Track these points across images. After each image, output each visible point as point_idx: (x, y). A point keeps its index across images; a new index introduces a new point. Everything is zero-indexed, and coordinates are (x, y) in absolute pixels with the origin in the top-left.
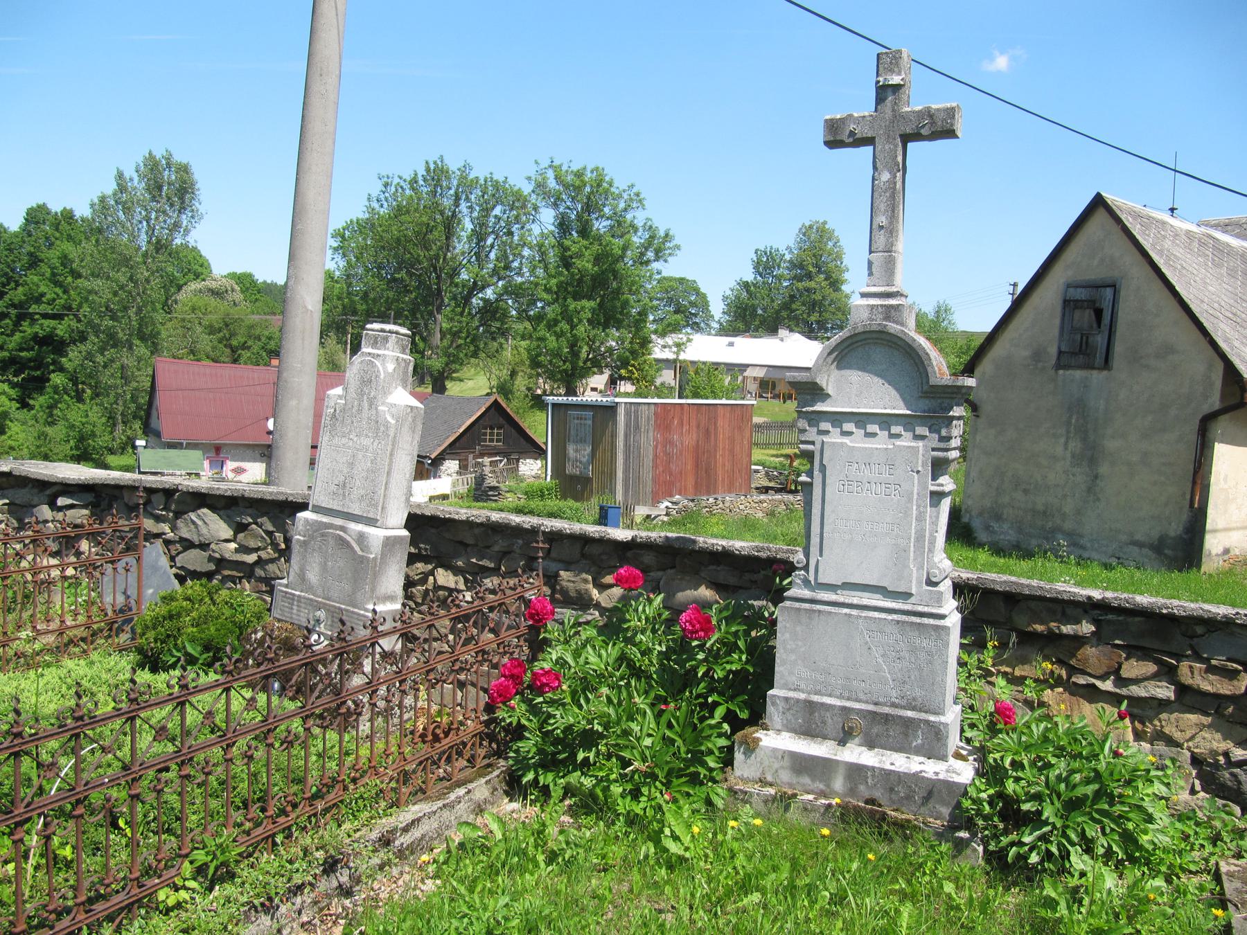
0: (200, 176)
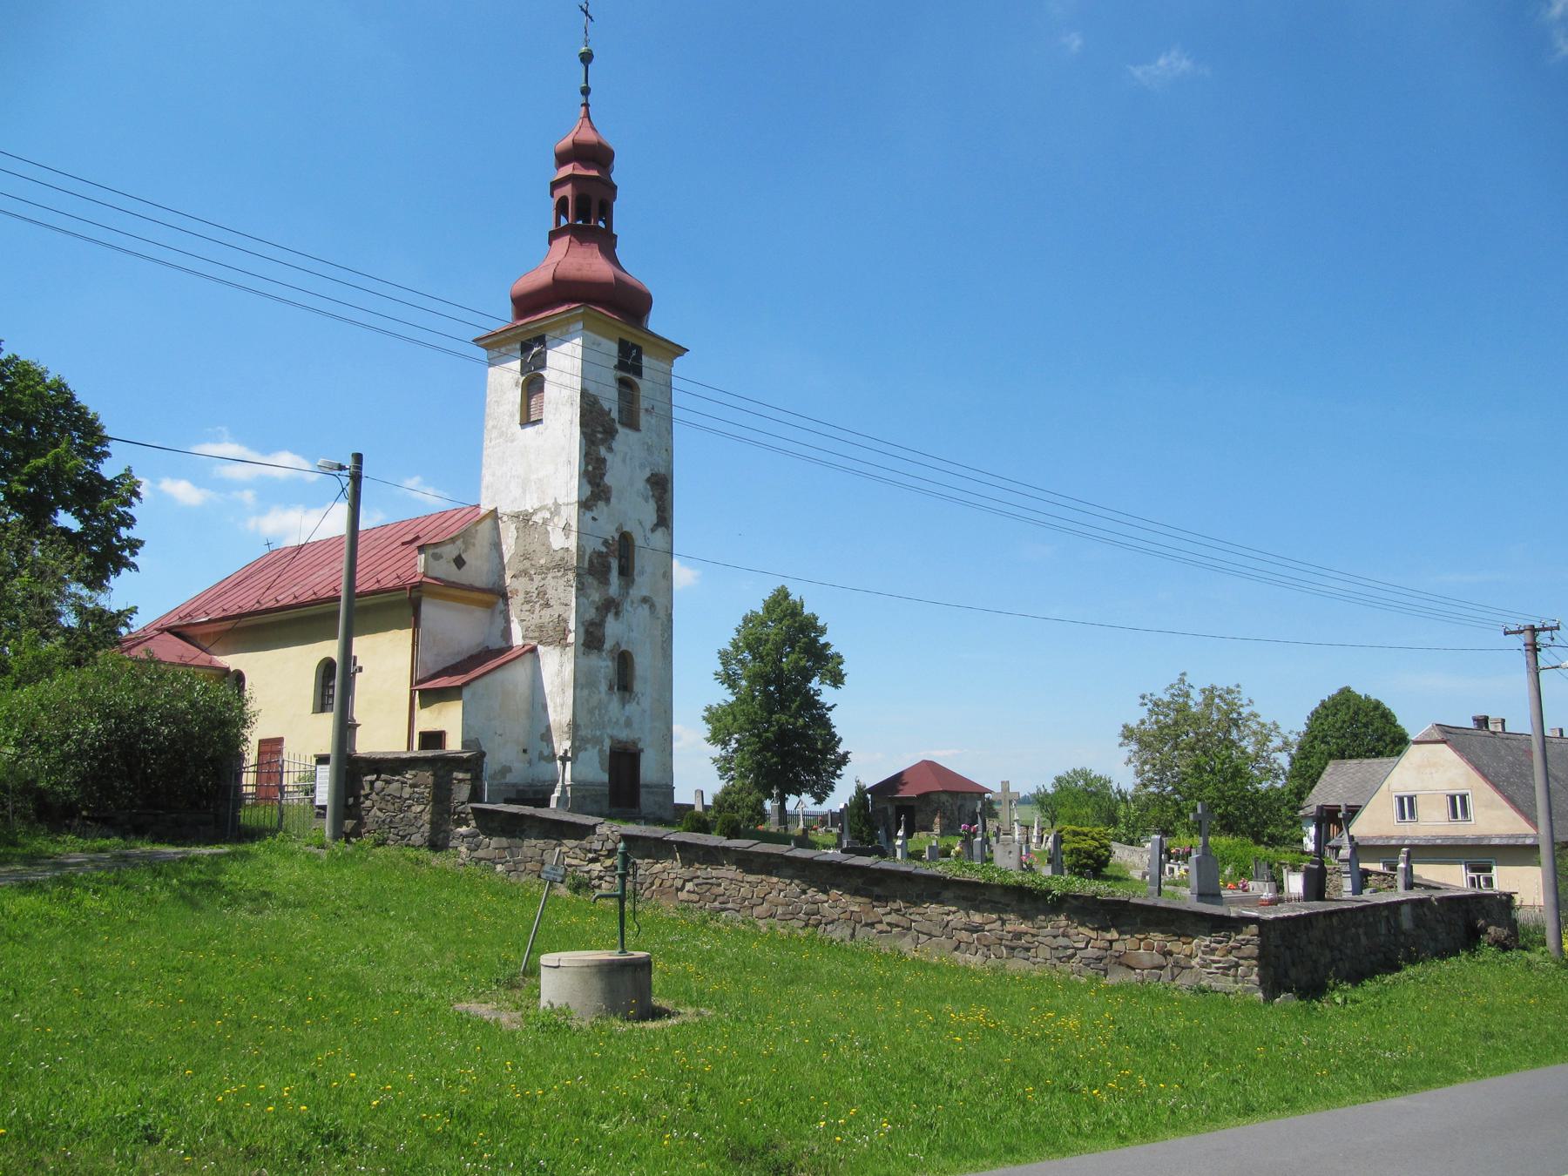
0: (1364, 688)
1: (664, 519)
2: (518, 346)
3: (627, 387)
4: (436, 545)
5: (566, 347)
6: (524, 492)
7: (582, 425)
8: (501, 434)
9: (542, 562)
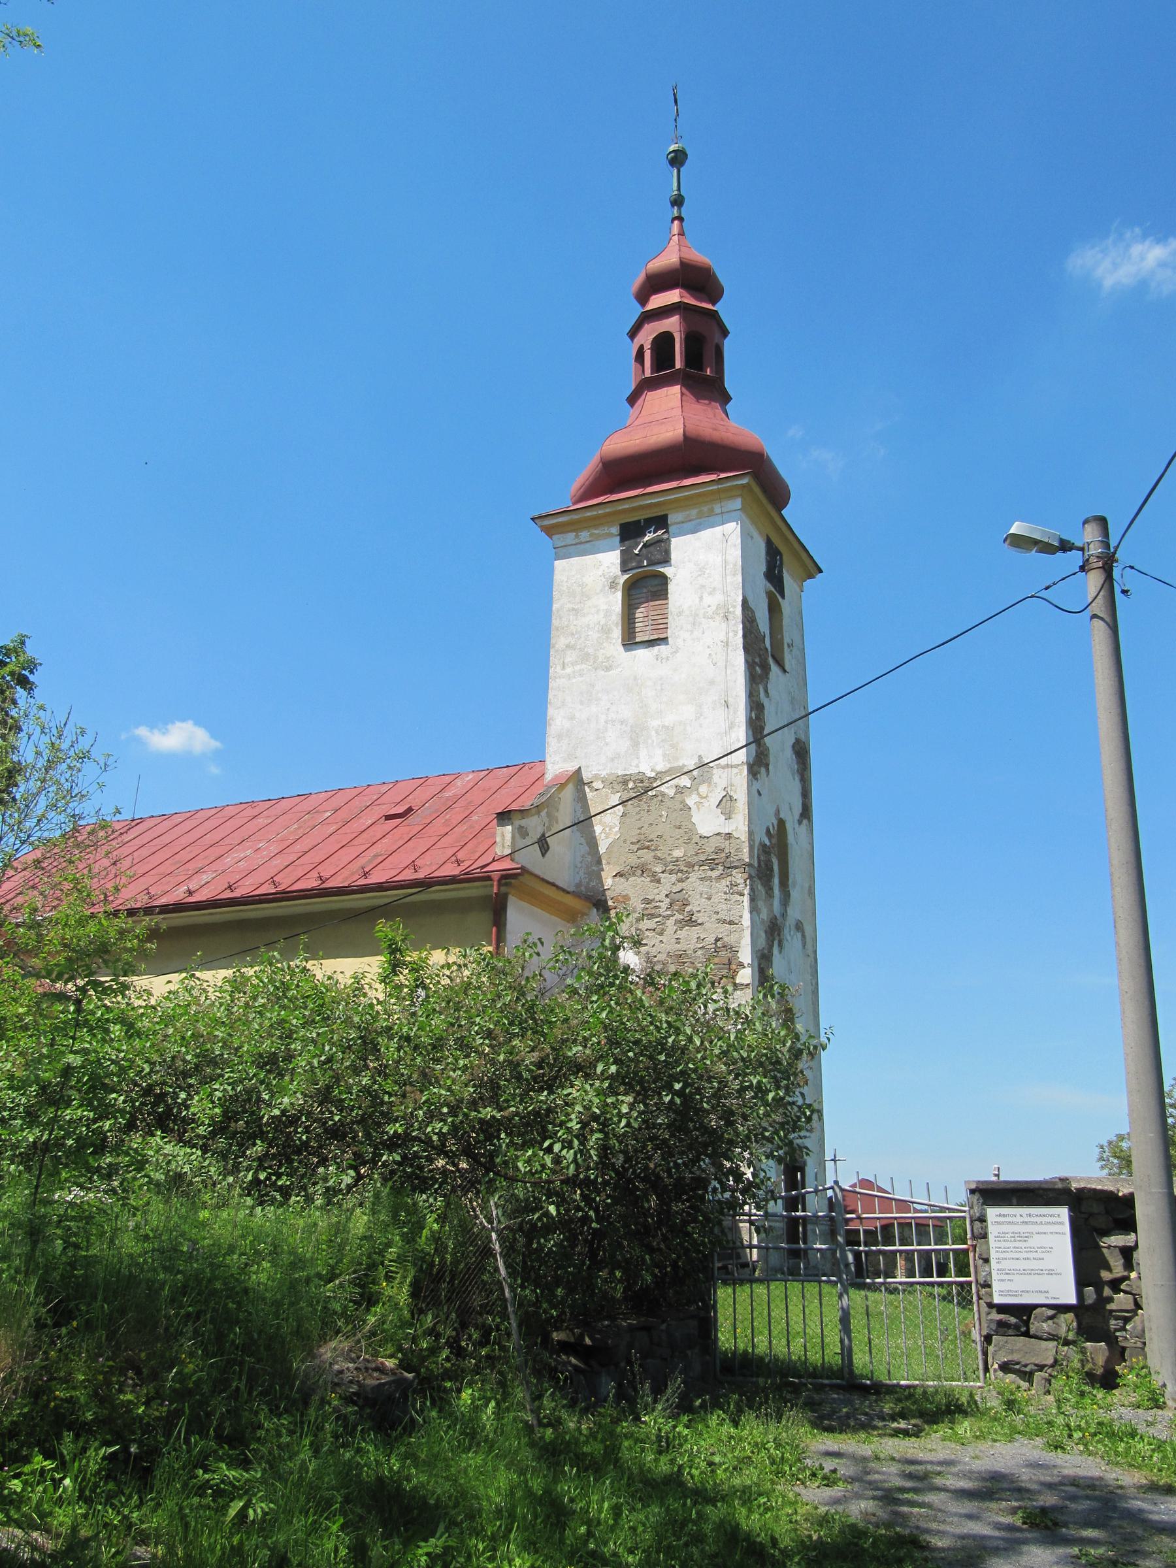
1: (806, 813)
2: (615, 530)
3: (774, 609)
4: (523, 812)
5: (710, 535)
6: (636, 744)
7: (745, 648)
8: (585, 658)
9: (678, 853)
